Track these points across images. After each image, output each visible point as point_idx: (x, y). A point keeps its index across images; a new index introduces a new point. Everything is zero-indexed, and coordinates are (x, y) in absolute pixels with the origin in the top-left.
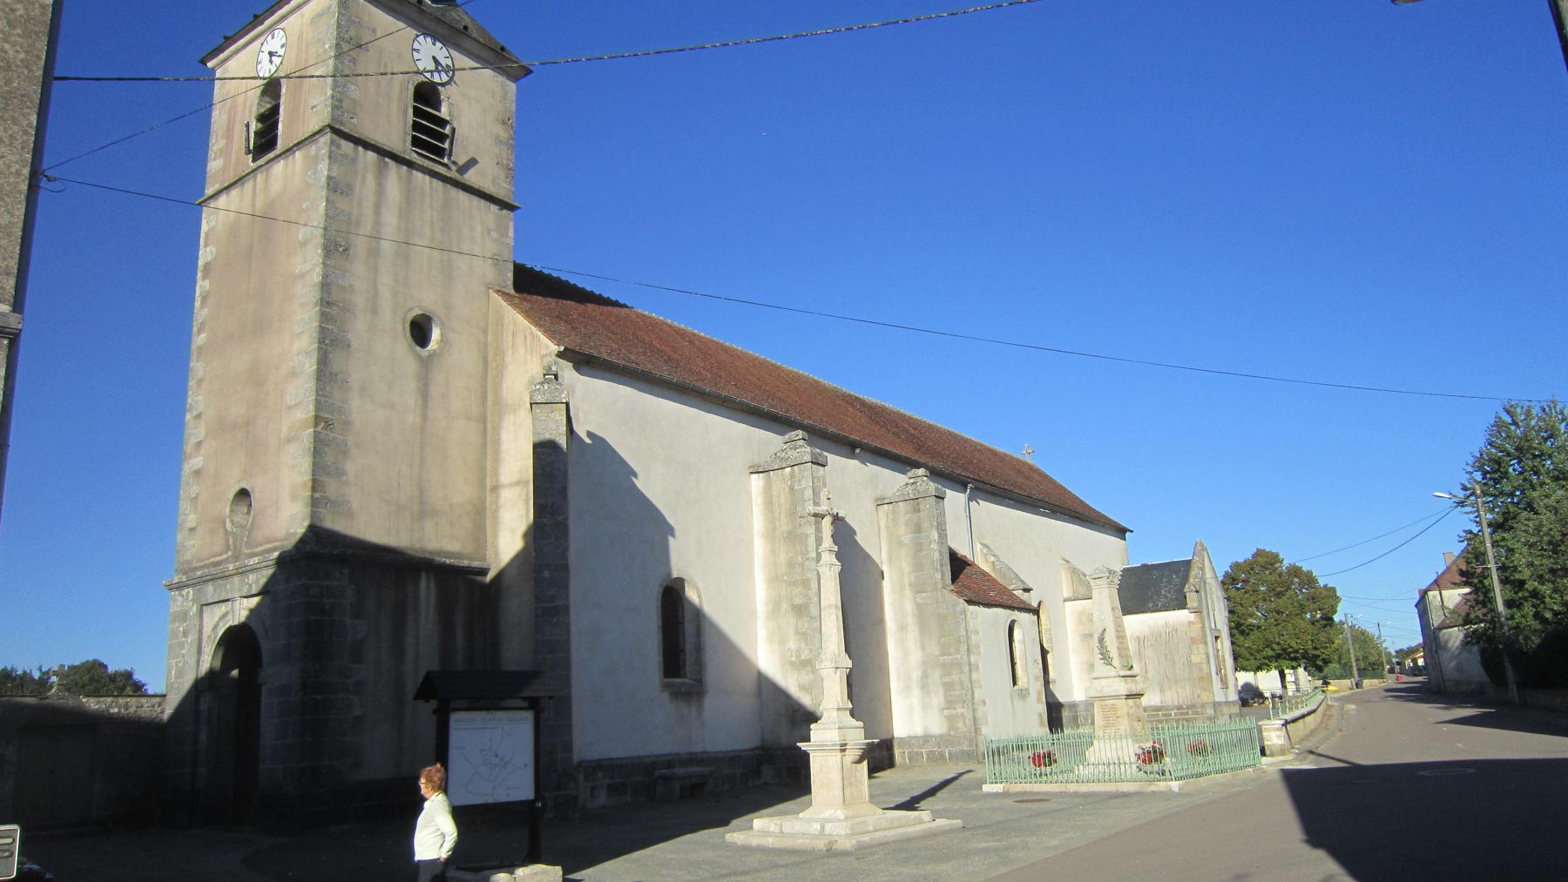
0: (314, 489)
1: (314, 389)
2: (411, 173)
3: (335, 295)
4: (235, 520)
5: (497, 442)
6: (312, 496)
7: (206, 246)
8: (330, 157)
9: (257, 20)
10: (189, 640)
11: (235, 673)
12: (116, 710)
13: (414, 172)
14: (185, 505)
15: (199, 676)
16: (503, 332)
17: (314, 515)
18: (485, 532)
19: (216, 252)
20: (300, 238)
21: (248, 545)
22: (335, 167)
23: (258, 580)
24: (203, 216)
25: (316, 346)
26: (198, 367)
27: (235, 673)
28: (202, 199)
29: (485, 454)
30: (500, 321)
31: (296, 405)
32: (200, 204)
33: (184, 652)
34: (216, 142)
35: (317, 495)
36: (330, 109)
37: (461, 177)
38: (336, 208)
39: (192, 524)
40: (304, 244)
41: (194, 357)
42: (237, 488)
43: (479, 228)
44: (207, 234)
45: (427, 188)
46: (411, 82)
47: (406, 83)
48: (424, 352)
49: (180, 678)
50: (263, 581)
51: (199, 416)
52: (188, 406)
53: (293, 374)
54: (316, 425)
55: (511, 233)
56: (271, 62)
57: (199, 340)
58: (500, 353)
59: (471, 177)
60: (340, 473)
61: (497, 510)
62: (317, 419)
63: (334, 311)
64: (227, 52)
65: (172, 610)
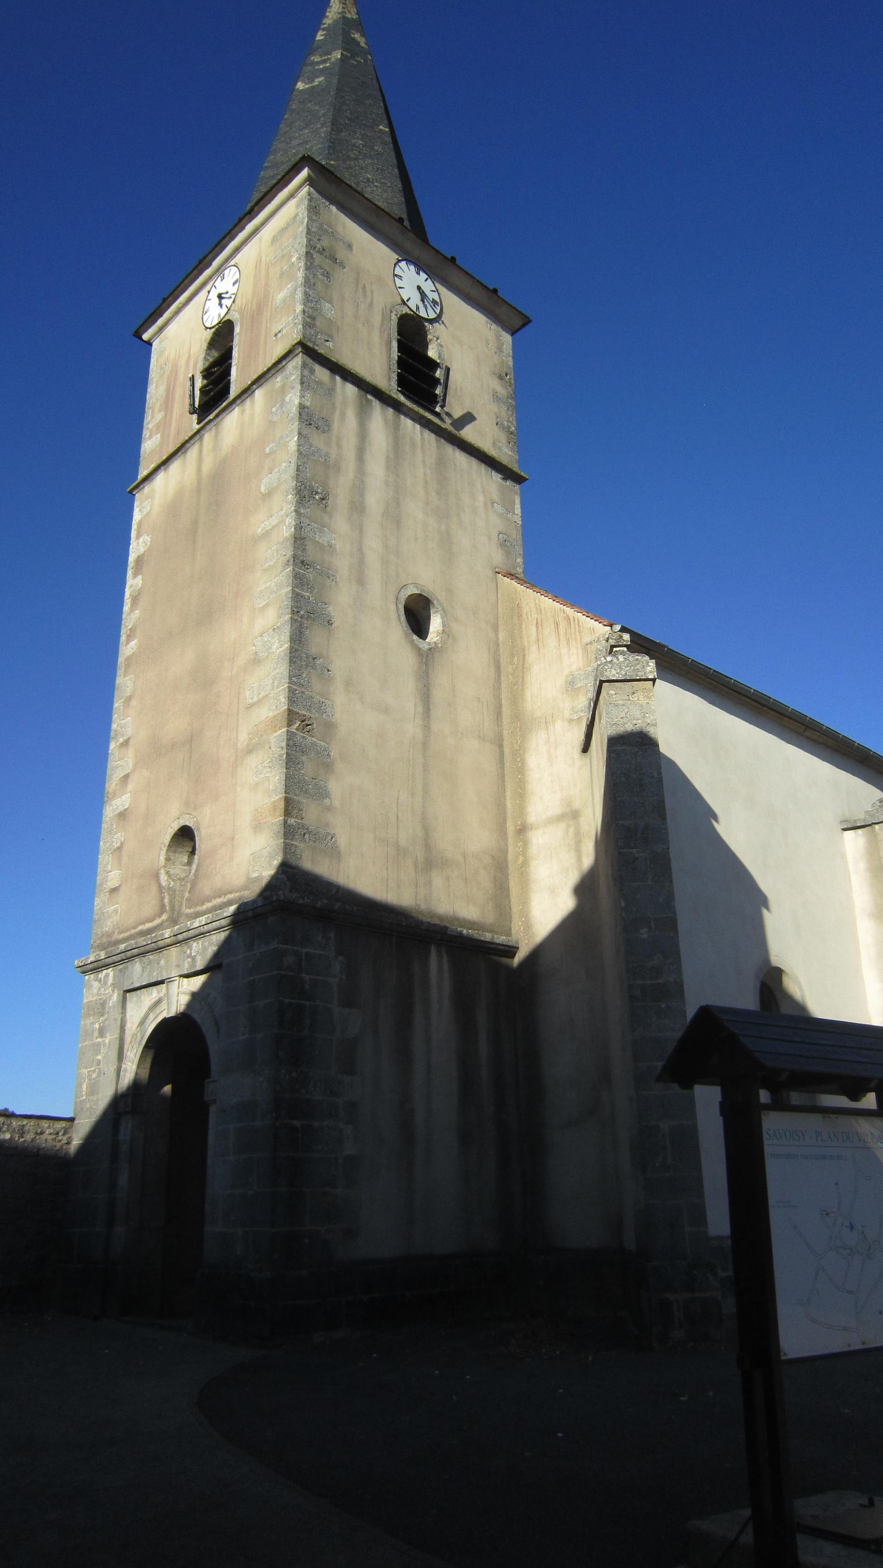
0: (287, 813)
1: (286, 674)
2: (399, 419)
3: (311, 553)
4: (172, 872)
5: (521, 770)
6: (285, 822)
7: (138, 537)
8: (302, 383)
9: (202, 264)
10: (107, 1041)
11: (167, 1089)
12: (8, 1136)
13: (402, 417)
14: (105, 860)
15: (120, 1091)
16: (521, 624)
17: (287, 849)
18: (508, 896)
19: (151, 542)
20: (263, 489)
21: (191, 903)
22: (308, 395)
23: (205, 948)
24: (136, 504)
25: (287, 617)
26: (125, 682)
27: (167, 1089)
28: (135, 484)
29: (504, 790)
30: (516, 611)
31: (259, 702)
32: (131, 492)
33: (99, 1057)
34: (153, 417)
35: (291, 821)
36: (300, 326)
37: (457, 432)
38: (311, 446)
39: (113, 883)
40: (269, 495)
41: (120, 672)
42: (176, 827)
43: (481, 498)
44: (140, 524)
45: (418, 437)
46: (394, 312)
47: (389, 313)
48: (424, 645)
49: (93, 1095)
50: (212, 950)
51: (126, 743)
52: (112, 734)
53: (256, 661)
54: (290, 723)
55: (518, 509)
56: (221, 305)
57: (128, 649)
58: (519, 653)
59: (468, 433)
60: (322, 794)
61: (525, 864)
62: (291, 716)
63: (311, 575)
64: (166, 315)
65: (85, 1001)
